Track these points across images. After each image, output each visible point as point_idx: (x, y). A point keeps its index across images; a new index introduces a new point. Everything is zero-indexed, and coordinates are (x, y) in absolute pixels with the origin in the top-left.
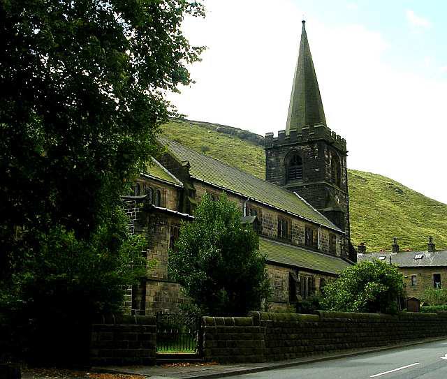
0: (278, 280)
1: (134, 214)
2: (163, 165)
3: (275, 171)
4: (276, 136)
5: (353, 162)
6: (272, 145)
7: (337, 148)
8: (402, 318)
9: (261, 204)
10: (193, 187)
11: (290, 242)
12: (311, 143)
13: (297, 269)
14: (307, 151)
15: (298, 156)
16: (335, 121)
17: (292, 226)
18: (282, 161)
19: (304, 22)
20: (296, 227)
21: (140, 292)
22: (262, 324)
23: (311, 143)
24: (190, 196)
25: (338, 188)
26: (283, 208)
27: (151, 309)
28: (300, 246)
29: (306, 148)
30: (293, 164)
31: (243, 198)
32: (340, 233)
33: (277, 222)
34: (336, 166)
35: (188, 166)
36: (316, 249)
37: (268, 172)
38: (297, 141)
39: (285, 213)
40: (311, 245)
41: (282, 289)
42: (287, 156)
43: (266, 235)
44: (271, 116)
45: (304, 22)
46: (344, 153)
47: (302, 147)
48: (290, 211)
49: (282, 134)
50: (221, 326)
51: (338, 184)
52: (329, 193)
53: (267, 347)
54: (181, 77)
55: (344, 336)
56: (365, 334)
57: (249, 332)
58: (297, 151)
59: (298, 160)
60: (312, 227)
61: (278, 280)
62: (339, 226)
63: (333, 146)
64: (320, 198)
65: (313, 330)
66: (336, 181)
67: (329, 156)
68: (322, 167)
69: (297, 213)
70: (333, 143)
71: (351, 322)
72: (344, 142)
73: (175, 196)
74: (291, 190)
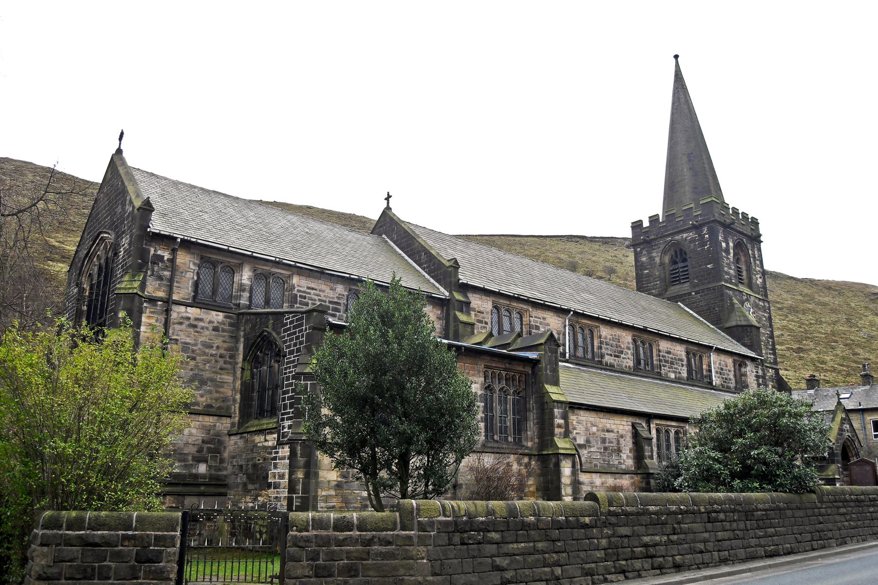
0: (608, 435)
1: (303, 335)
2: (423, 269)
3: (648, 275)
4: (646, 224)
5: (778, 255)
6: (643, 236)
7: (747, 234)
8: (825, 498)
9: (597, 319)
10: (467, 297)
11: (659, 376)
12: (697, 228)
13: (649, 417)
14: (693, 240)
15: (681, 250)
16: (738, 193)
17: (659, 351)
18: (657, 260)
19: (676, 57)
20: (669, 353)
21: (302, 463)
22: (422, 527)
23: (697, 228)
24: (461, 311)
25: (747, 291)
26: (639, 323)
27: (333, 493)
28: (678, 381)
29: (691, 235)
30: (675, 263)
31: (561, 311)
32: (753, 359)
33: (631, 346)
34: (743, 259)
35: (456, 265)
36: (710, 385)
37: (639, 278)
38: (678, 227)
39: (644, 330)
40: (646, 368)
41: (619, 451)
42: (664, 252)
43: (612, 366)
44: (628, 195)
45: (676, 57)
46: (756, 239)
47: (685, 235)
48: (652, 326)
49: (654, 219)
50: (324, 533)
51: (750, 286)
52: (731, 300)
53: (434, 574)
54: (641, 221)
55: (672, 542)
56: (727, 535)
57: (389, 543)
58: (678, 243)
59: (681, 255)
60: (698, 350)
61: (608, 435)
62: (750, 347)
63: (732, 229)
64: (716, 312)
65: (579, 533)
66: (746, 281)
67: (728, 244)
68: (716, 260)
69: (665, 329)
70: (733, 223)
71: (686, 512)
72: (755, 222)
73: (439, 312)
74: (674, 299)
